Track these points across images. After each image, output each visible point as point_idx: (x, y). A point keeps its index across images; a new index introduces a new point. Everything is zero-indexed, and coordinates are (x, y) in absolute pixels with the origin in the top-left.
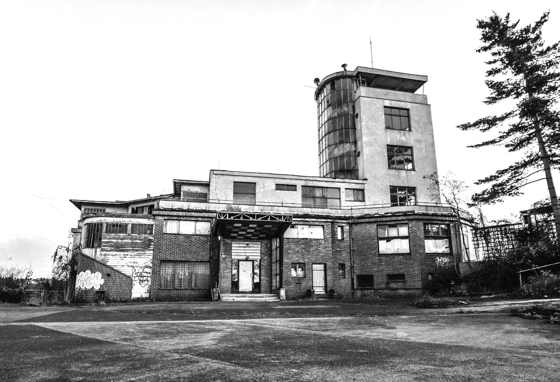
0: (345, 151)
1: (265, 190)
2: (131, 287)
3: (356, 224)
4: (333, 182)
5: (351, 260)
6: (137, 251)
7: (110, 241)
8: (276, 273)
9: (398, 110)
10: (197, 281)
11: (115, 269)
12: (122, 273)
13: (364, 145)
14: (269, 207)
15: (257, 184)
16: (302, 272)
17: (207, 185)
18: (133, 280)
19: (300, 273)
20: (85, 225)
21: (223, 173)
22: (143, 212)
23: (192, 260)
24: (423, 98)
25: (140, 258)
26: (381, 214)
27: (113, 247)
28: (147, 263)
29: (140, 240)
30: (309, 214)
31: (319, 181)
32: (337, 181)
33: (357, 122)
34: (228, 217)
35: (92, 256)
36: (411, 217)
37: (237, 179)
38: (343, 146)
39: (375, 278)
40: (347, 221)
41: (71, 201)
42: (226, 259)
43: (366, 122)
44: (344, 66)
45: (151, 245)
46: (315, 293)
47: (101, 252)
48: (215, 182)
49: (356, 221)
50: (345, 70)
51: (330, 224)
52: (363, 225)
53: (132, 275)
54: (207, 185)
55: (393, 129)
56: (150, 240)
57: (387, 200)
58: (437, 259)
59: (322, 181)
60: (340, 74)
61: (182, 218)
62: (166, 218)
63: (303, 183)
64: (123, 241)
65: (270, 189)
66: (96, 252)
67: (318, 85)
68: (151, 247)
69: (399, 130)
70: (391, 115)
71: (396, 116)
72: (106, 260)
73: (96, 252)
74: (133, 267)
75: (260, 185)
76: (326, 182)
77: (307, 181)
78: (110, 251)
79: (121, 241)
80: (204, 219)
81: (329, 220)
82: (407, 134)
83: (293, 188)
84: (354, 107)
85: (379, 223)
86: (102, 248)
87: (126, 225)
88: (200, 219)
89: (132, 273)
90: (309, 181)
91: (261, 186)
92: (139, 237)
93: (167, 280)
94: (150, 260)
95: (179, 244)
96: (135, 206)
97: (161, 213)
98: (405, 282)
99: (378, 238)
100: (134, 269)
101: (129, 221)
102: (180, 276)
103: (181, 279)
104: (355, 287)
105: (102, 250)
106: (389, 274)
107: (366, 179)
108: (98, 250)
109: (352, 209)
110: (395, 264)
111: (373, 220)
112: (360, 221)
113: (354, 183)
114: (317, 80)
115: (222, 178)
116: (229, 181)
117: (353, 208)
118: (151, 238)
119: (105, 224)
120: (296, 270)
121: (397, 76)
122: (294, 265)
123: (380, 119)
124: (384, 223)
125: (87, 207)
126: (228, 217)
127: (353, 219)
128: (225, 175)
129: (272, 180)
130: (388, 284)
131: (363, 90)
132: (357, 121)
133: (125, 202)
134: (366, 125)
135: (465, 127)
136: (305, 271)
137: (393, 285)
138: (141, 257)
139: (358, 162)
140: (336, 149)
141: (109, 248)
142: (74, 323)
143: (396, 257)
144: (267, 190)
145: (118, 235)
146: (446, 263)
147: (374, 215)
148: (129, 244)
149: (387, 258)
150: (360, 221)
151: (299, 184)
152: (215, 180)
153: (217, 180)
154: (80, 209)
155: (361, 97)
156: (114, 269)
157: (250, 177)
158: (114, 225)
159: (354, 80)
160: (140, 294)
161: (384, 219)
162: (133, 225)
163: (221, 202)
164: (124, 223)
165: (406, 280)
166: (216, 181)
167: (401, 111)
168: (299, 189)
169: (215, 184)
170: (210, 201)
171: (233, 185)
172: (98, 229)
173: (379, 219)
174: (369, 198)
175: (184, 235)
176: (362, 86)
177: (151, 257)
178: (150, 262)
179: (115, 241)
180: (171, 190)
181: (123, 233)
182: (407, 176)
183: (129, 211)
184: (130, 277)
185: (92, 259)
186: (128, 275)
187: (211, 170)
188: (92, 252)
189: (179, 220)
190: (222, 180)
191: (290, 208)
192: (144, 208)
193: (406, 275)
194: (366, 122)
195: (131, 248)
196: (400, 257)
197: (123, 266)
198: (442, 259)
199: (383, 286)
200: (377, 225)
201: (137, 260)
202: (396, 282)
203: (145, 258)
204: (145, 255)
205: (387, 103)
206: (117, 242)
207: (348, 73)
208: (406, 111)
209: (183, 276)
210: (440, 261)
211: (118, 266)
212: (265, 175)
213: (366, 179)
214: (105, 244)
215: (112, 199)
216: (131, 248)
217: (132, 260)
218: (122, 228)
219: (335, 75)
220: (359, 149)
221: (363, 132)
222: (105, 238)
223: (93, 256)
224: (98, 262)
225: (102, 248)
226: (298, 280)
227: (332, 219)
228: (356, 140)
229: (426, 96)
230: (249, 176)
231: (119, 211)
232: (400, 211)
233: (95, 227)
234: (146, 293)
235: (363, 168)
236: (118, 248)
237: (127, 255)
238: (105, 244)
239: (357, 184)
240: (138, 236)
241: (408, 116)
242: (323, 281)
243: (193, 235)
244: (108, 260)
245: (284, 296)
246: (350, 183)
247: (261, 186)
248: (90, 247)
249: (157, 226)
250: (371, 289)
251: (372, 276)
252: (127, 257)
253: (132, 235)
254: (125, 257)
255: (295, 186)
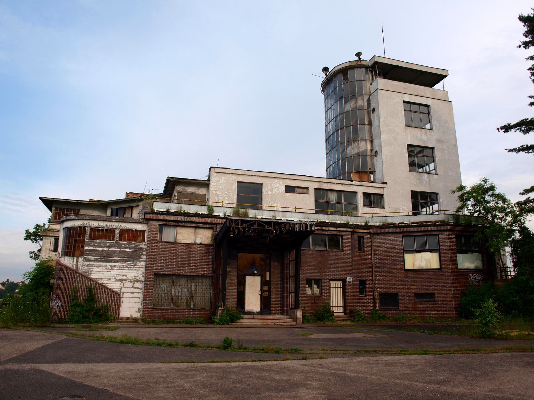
0: (361, 150)
1: (274, 192)
2: (119, 305)
3: (378, 234)
4: (349, 185)
5: (372, 275)
6: (126, 261)
7: (95, 248)
8: (290, 291)
9: (409, 105)
10: (196, 299)
11: (100, 282)
12: (108, 288)
13: (383, 144)
14: (281, 213)
15: (264, 185)
16: (317, 289)
17: (206, 184)
18: (121, 296)
19: (316, 290)
20: (64, 229)
21: (224, 171)
22: (124, 214)
23: (191, 274)
24: (444, 94)
25: (129, 270)
26: (407, 224)
27: (98, 257)
28: (138, 276)
29: (130, 248)
30: (326, 221)
31: (335, 183)
32: (354, 184)
33: (374, 117)
34: (240, 224)
35: (73, 266)
36: (443, 228)
37: (242, 179)
38: (358, 144)
39: (400, 297)
40: (368, 231)
41: (41, 198)
42: (230, 274)
43: (385, 118)
44: (358, 54)
45: (142, 255)
46: (335, 314)
47: (84, 262)
48: (215, 181)
49: (379, 231)
50: (360, 59)
51: (350, 233)
52: (387, 236)
53: (120, 290)
54: (206, 184)
55: (412, 127)
56: (141, 249)
57: (408, 206)
58: (470, 276)
59: (337, 183)
60: (354, 64)
61: (180, 224)
62: (161, 223)
63: (317, 185)
64: (110, 249)
65: (278, 191)
66: (77, 262)
67: (326, 74)
68: (142, 257)
69: (420, 128)
70: (411, 111)
71: (416, 112)
72: (89, 272)
73: (77, 262)
74: (121, 281)
75: (267, 186)
76: (342, 184)
77: (321, 183)
78: (94, 261)
79: (107, 249)
80: (205, 226)
81: (348, 230)
82: (428, 133)
83: (305, 190)
84: (369, 100)
85: (406, 234)
86: (85, 257)
87: (114, 231)
88: (201, 225)
89: (120, 287)
90: (323, 183)
91: (269, 187)
92: (129, 245)
93: (162, 298)
94: (142, 273)
95: (176, 255)
96: (115, 207)
97: (155, 217)
98: (435, 301)
99: (404, 251)
100: (122, 284)
101: (117, 226)
102: (177, 293)
103: (179, 296)
104: (377, 308)
105: (86, 260)
106: (416, 292)
107: (386, 183)
108: (80, 259)
109: (372, 217)
110: (424, 281)
111: (398, 230)
112: (383, 231)
113: (372, 187)
114: (325, 69)
115: (224, 177)
116: (232, 180)
117: (374, 215)
118: (143, 247)
119: (89, 229)
120: (311, 287)
121: (416, 68)
122: (309, 282)
123: (400, 115)
124: (410, 234)
125: (58, 206)
126: (240, 224)
127: (375, 229)
128: (228, 173)
129: (281, 181)
130: (415, 303)
131: (381, 82)
132: (374, 116)
133: (104, 201)
134: (384, 121)
135: (507, 128)
136: (322, 288)
137: (421, 306)
138: (131, 269)
139: (375, 163)
140: (350, 147)
141: (93, 258)
142: (337, 360)
143: (424, 273)
144: (275, 192)
145: (103, 242)
146: (480, 280)
147: (399, 224)
148: (117, 253)
149: (415, 274)
150: (383, 231)
151: (312, 186)
152: (216, 179)
153: (218, 179)
154: (51, 210)
155: (378, 90)
156: (99, 283)
157: (256, 177)
158: (99, 230)
159: (369, 70)
160: (130, 314)
161: (411, 229)
162: (122, 231)
163: (225, 205)
164: (111, 227)
165: (437, 299)
166: (217, 180)
167: (421, 107)
168: (312, 192)
169: (216, 184)
170: (264, 208)
171: (236, 186)
172: (80, 234)
173: (405, 230)
174: (389, 205)
175: (182, 243)
176: (380, 78)
177: (143, 270)
178: (141, 275)
179: (100, 249)
180: (160, 190)
181: (109, 239)
182: (429, 180)
183: (108, 212)
184: (117, 293)
185: (72, 270)
186: (115, 290)
187: (211, 167)
188: (73, 262)
189: (177, 226)
190: (224, 180)
191: (304, 214)
192: (126, 209)
193: (436, 294)
194: (385, 118)
195: (119, 258)
196: (429, 273)
197: (110, 279)
198: (475, 276)
199: (410, 306)
200: (403, 236)
201: (127, 272)
202: (425, 302)
203: (135, 270)
204: (135, 266)
205: (407, 98)
206: (103, 251)
207: (363, 63)
208: (426, 108)
209: (180, 293)
210: (473, 278)
211: (104, 280)
212: (273, 175)
213: (386, 183)
214: (88, 253)
215: (85, 198)
216: (119, 258)
217: (119, 272)
218: (108, 234)
219: (348, 65)
220: (376, 148)
221: (381, 129)
222: (89, 245)
223: (75, 266)
224: (80, 274)
225: (85, 257)
226: (314, 299)
227: (352, 228)
228: (372, 138)
229: (447, 92)
230: (255, 176)
231: (96, 213)
232: (429, 221)
233: (77, 232)
234: (136, 312)
235: (381, 169)
236: (104, 257)
237: (115, 266)
238: (88, 253)
239: (376, 188)
240: (128, 243)
241: (429, 114)
242: (342, 300)
243: (193, 244)
244: (92, 272)
245: (300, 318)
246: (368, 186)
247: (269, 187)
248: (70, 256)
249: (150, 232)
250: (395, 310)
251: (397, 295)
252: (115, 268)
253: (121, 242)
254: (112, 269)
255: (307, 188)
